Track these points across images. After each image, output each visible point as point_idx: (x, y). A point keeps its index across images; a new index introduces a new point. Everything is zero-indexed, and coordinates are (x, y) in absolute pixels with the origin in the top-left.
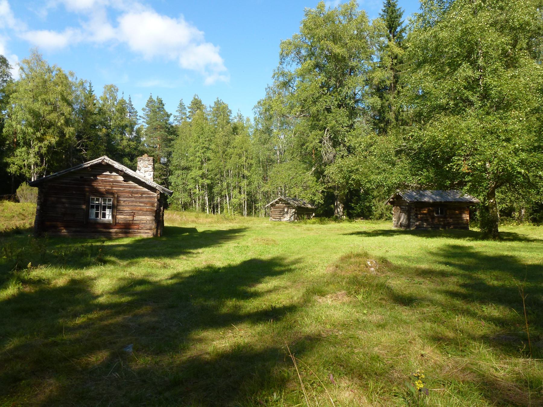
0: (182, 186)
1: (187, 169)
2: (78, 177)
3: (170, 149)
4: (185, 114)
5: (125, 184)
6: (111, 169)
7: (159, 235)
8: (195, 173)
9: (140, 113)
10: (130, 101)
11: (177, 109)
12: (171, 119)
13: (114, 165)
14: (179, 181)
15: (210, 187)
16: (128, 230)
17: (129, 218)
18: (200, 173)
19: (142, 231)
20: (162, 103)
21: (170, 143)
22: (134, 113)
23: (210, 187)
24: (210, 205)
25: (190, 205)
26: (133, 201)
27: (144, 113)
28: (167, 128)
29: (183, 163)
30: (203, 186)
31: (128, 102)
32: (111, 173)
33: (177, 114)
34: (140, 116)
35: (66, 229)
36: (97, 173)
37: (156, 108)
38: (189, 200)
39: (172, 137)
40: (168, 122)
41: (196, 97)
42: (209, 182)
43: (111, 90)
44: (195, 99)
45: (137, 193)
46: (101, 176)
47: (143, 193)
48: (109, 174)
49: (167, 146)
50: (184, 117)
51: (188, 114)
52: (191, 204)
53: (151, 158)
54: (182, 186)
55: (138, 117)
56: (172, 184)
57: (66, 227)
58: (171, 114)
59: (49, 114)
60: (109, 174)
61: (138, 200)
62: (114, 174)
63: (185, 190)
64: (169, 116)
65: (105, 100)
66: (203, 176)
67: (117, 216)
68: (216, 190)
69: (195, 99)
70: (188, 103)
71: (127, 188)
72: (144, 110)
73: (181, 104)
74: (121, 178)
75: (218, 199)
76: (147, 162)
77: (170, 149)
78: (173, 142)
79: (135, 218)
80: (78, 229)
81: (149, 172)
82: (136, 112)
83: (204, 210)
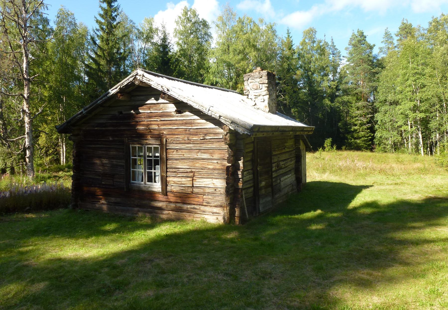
0: (390, 123)
1: (396, 103)
2: (116, 113)
3: (374, 84)
4: (392, 43)
5: (178, 117)
6: (158, 94)
7: (237, 220)
8: (406, 106)
9: (344, 53)
10: (333, 43)
11: (382, 40)
12: (375, 51)
13: (150, 83)
14: (387, 119)
15: (425, 122)
16: (185, 207)
17: (187, 182)
18: (412, 104)
19: (207, 209)
20: (363, 35)
21: (375, 76)
22: (336, 53)
23: (425, 122)
24: (424, 144)
25: (401, 144)
26: (191, 150)
27: (347, 52)
28: (371, 61)
29: (390, 97)
30: (416, 122)
31: (330, 44)
32: (157, 99)
33: (383, 45)
34: (343, 57)
35: (106, 200)
36: (138, 103)
37: (360, 41)
38: (400, 138)
39: (376, 70)
40: (371, 55)
41: (405, 22)
42: (422, 115)
43: (310, 33)
44: (403, 24)
45: (196, 134)
46: (144, 107)
47: (207, 132)
48: (155, 102)
49: (370, 80)
50: (391, 47)
51: (396, 43)
52: (402, 144)
53: (265, 73)
54: (390, 123)
55: (341, 58)
56: (379, 123)
57: (106, 195)
58: (374, 45)
59: (239, 62)
60: (155, 102)
61: (198, 146)
62: (161, 101)
63: (393, 129)
64: (371, 48)
65: (304, 43)
66: (415, 109)
67: (168, 179)
68: (433, 125)
69: (403, 24)
70: (394, 29)
71: (182, 124)
72: (346, 49)
73: (386, 33)
74: (172, 108)
75: (436, 136)
76: (258, 80)
77: (374, 84)
78: (377, 76)
79: (196, 184)
80: (119, 200)
81: (261, 97)
82: (339, 52)
83: (417, 150)
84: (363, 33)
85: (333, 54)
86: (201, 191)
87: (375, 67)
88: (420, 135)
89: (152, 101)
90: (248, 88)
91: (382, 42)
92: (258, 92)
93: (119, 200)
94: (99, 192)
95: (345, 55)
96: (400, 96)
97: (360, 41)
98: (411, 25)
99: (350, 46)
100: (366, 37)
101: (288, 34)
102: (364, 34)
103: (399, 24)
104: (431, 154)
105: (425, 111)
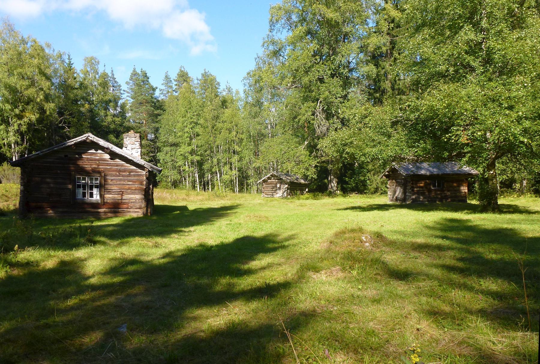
0: (171, 163)
3: (157, 125)
4: (171, 87)
5: (112, 162)
6: (97, 146)
7: (149, 214)
8: (184, 149)
9: (124, 87)
10: (113, 75)
11: (163, 82)
12: (157, 93)
14: (168, 158)
15: (200, 164)
17: (118, 197)
18: (189, 149)
19: (131, 210)
20: (146, 76)
21: (157, 118)
23: (200, 164)
24: (200, 182)
25: (180, 182)
26: (120, 180)
27: (128, 86)
28: (153, 102)
29: (171, 139)
31: (110, 75)
33: (163, 87)
34: (124, 91)
35: (52, 210)
40: (153, 96)
41: (182, 69)
42: (198, 158)
44: (181, 71)
45: (125, 171)
46: (86, 154)
47: (131, 171)
48: (95, 152)
49: (153, 122)
50: (170, 90)
52: (181, 182)
53: (138, 135)
55: (122, 92)
56: (161, 161)
57: (52, 208)
58: (157, 88)
59: (27, 89)
61: (126, 178)
63: (174, 168)
64: (154, 90)
65: (86, 73)
66: (192, 152)
67: (105, 196)
68: (206, 166)
69: (181, 71)
70: (174, 76)
71: (114, 166)
72: (127, 83)
73: (166, 77)
74: (107, 156)
75: (208, 176)
76: (134, 139)
77: (157, 125)
78: (159, 117)
79: (124, 197)
80: (66, 210)
81: (136, 149)
82: (120, 86)
83: (194, 187)
84: (146, 74)
85: (113, 86)
86: (127, 201)
87: (157, 108)
88: (197, 175)
89: (93, 151)
90: (127, 143)
91: (162, 84)
92: (134, 146)
93: (66, 210)
94: (45, 205)
95: (126, 89)
96: (179, 140)
97: (141, 81)
98: (187, 74)
99: (131, 82)
100: (148, 78)
101: (69, 59)
102: (147, 75)
103: (177, 71)
104: (205, 190)
105: (201, 155)
